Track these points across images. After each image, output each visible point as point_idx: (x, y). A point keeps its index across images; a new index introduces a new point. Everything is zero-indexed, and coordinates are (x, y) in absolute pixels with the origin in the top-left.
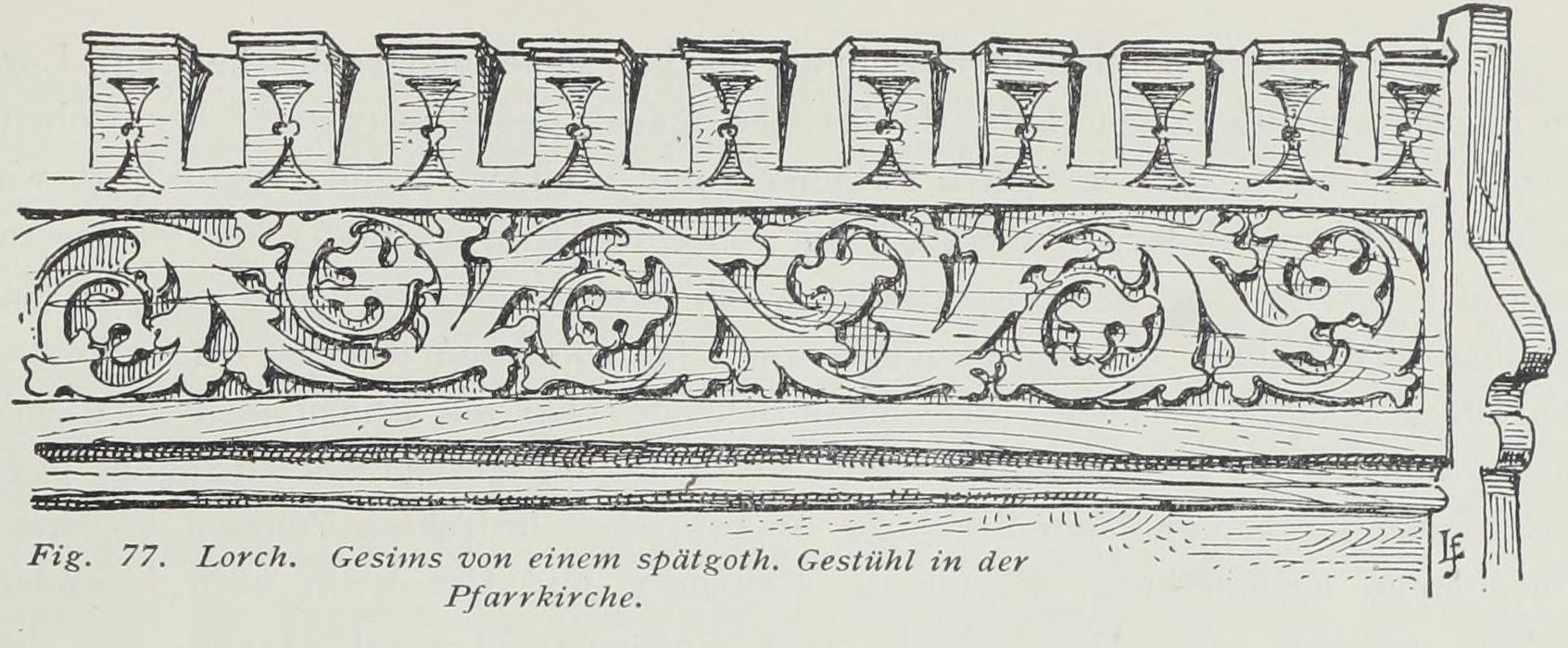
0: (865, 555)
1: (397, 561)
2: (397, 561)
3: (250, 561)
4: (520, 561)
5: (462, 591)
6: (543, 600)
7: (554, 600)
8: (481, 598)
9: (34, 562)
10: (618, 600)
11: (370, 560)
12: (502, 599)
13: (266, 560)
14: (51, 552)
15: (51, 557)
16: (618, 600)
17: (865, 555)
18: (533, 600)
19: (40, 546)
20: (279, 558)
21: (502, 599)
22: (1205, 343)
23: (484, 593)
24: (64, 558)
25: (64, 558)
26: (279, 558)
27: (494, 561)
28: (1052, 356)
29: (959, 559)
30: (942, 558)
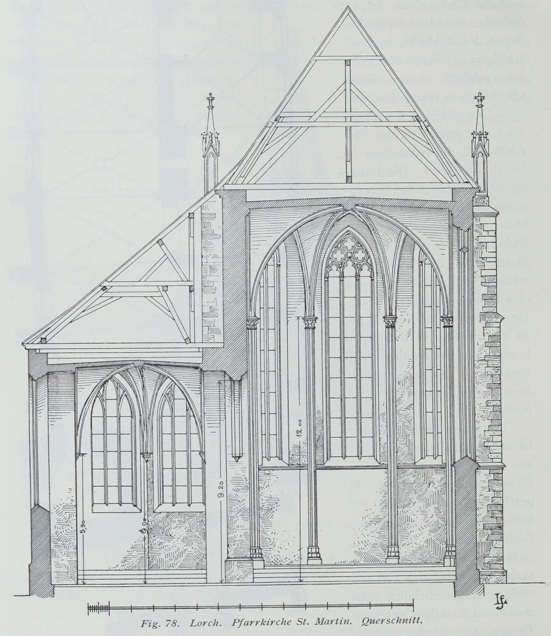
0: (340, 619)
1: (343, 622)
2: (343, 622)
3: (207, 624)
4: (357, 622)
5: (237, 621)
6: (263, 624)
7: (266, 623)
8: (243, 623)
9: (142, 626)
10: (286, 623)
11: (386, 621)
12: (330, 622)
13: (212, 624)
14: (148, 623)
15: (148, 624)
16: (286, 623)
17: (340, 619)
18: (259, 624)
19: (144, 621)
20: (216, 623)
21: (330, 622)
22: (254, 529)
23: (244, 621)
24: (152, 625)
25: (152, 625)
26: (216, 623)
27: (375, 621)
28: (83, 454)
29: (416, 620)
30: (270, 621)
